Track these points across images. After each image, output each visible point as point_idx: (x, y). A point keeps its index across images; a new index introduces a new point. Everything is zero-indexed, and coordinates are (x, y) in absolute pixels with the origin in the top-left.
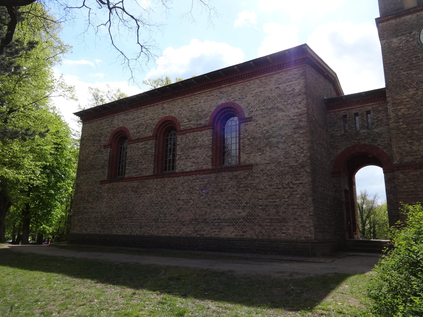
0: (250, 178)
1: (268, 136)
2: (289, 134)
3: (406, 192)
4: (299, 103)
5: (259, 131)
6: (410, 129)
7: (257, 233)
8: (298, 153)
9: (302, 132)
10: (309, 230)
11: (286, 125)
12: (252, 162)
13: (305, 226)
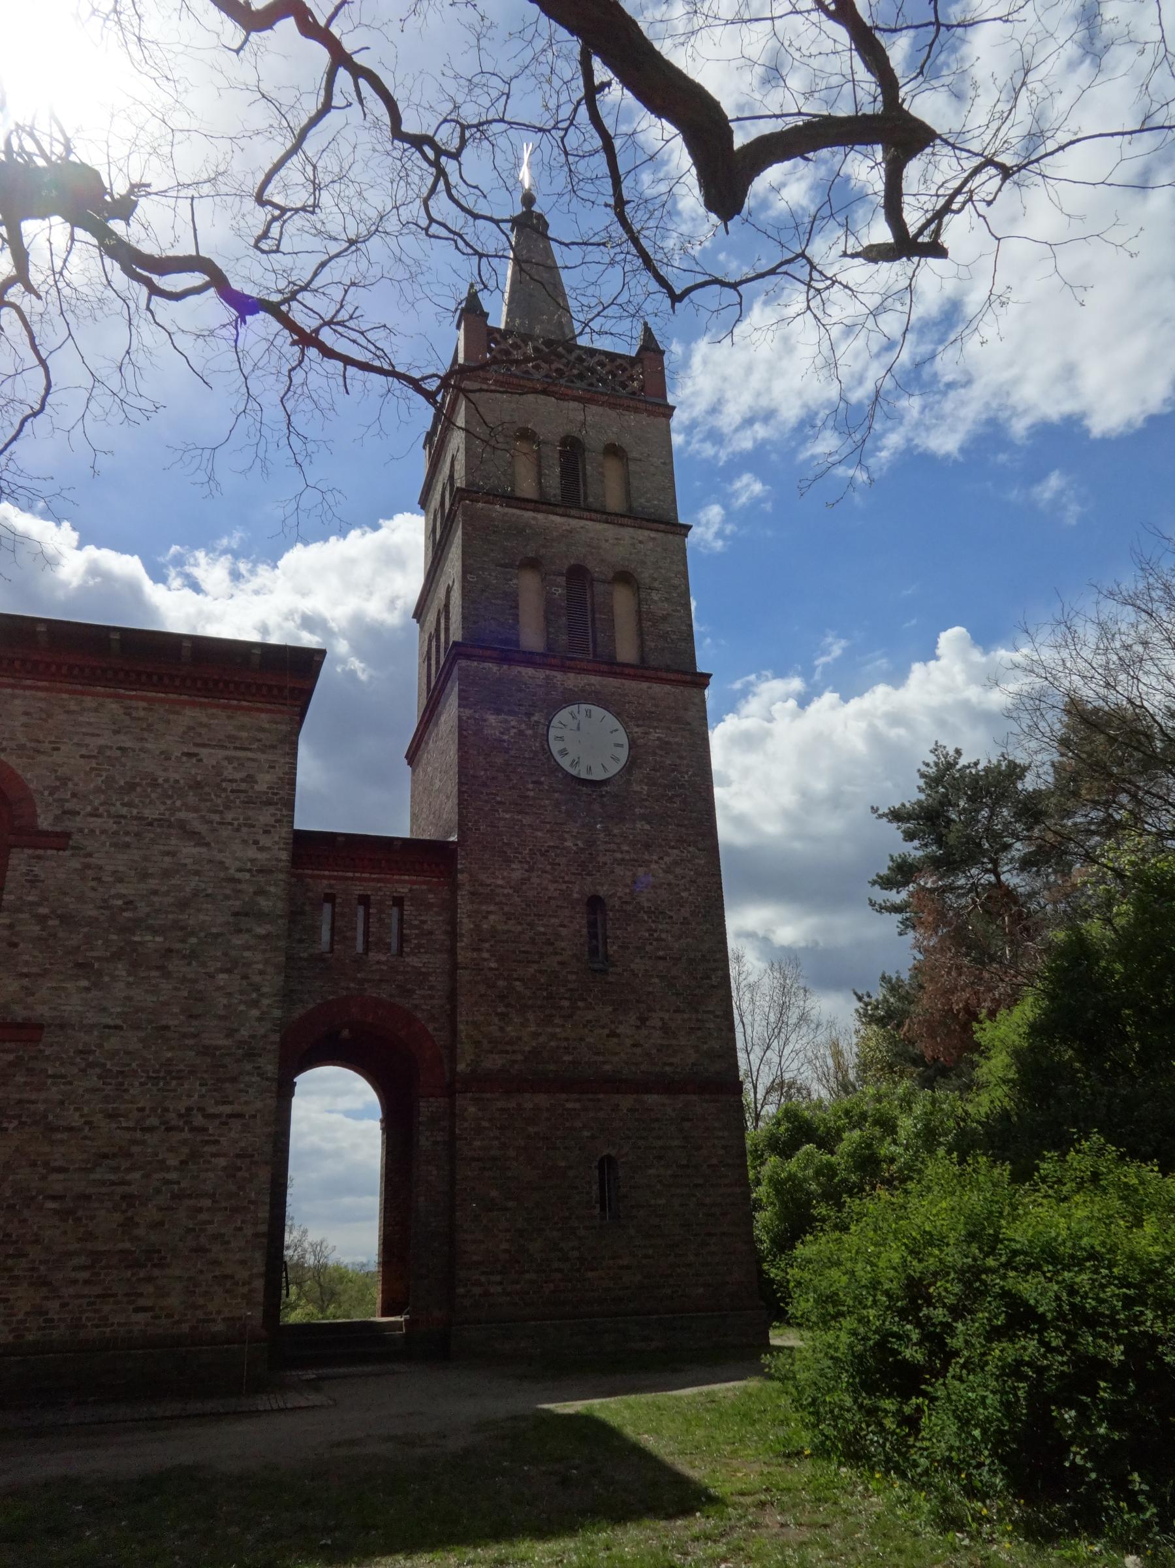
0: (20, 1079)
1: (129, 919)
2: (214, 930)
3: (478, 1160)
4: (265, 832)
5: (92, 894)
6: (506, 974)
7: (21, 1316)
8: (241, 1002)
9: (261, 931)
10: (245, 1290)
11: (207, 895)
12: (43, 1012)
13: (232, 1277)
